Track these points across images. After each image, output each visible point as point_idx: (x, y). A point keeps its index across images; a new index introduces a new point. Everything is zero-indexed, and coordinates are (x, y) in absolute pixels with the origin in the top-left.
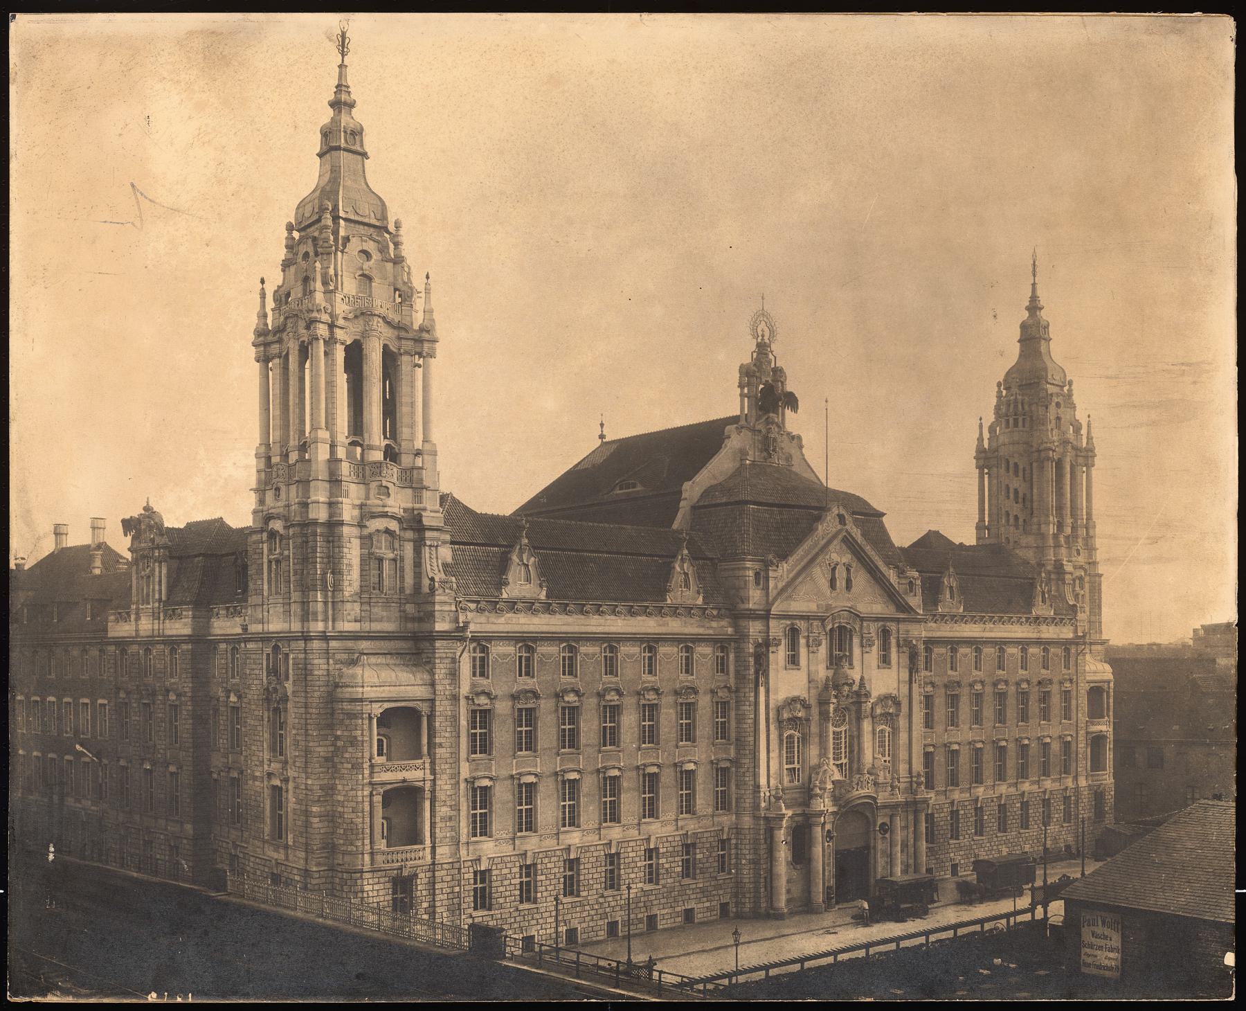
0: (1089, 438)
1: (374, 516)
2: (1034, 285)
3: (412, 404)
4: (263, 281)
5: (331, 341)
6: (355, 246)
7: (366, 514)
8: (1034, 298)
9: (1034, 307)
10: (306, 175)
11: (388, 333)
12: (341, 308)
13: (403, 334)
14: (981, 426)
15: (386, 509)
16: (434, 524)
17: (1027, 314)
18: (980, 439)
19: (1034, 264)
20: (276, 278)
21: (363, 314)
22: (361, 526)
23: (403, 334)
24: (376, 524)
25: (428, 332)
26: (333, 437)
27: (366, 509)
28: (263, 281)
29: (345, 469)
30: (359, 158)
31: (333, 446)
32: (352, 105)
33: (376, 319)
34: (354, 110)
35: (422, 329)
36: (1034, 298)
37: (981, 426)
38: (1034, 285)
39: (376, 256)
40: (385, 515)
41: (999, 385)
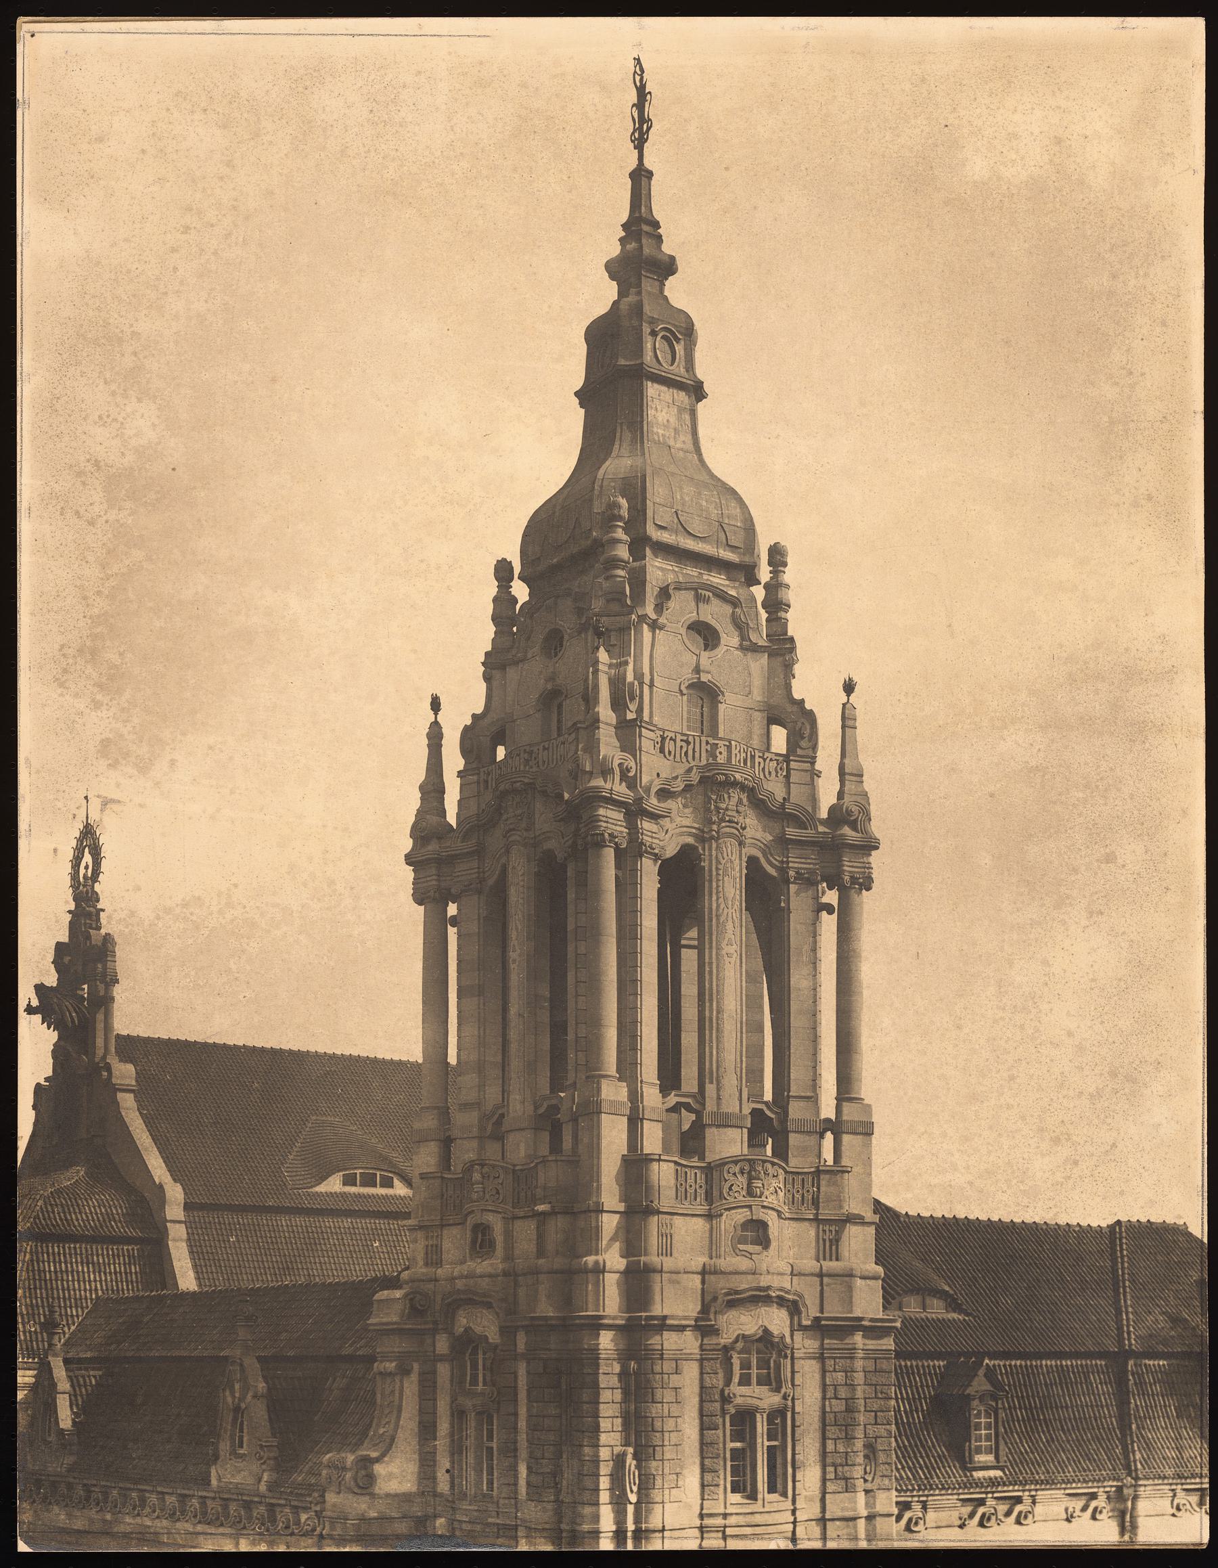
0: (848, 774)
1: (735, 1301)
2: (640, 177)
3: (814, 1014)
4: (436, 705)
5: (630, 854)
6: (682, 608)
7: (717, 1300)
8: (640, 225)
9: (642, 259)
10: (541, 452)
11: (755, 829)
12: (654, 767)
13: (792, 832)
14: (435, 736)
15: (764, 1281)
16: (177, 1226)
17: (609, 292)
18: (432, 789)
19: (641, 104)
20: (467, 699)
21: (710, 785)
22: (704, 1328)
23: (792, 832)
24: (745, 1322)
25: (854, 825)
26: (635, 1096)
27: (721, 1284)
28: (436, 705)
29: (663, 1174)
30: (681, 396)
31: (635, 1121)
32: (668, 268)
33: (735, 795)
34: (671, 282)
35: (838, 816)
36: (640, 225)
37: (435, 736)
38: (640, 177)
39: (729, 639)
40: (760, 1297)
41: (503, 571)
